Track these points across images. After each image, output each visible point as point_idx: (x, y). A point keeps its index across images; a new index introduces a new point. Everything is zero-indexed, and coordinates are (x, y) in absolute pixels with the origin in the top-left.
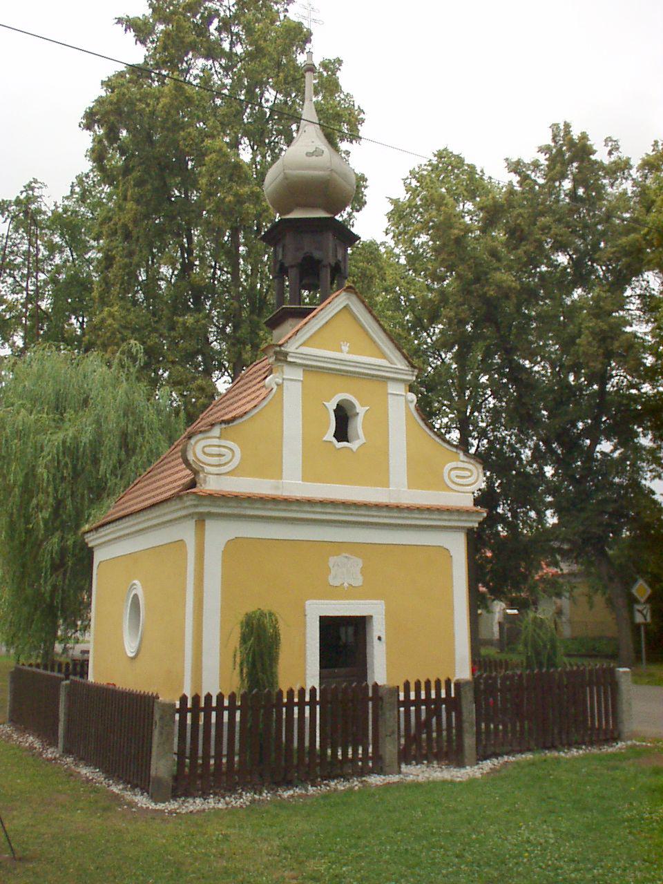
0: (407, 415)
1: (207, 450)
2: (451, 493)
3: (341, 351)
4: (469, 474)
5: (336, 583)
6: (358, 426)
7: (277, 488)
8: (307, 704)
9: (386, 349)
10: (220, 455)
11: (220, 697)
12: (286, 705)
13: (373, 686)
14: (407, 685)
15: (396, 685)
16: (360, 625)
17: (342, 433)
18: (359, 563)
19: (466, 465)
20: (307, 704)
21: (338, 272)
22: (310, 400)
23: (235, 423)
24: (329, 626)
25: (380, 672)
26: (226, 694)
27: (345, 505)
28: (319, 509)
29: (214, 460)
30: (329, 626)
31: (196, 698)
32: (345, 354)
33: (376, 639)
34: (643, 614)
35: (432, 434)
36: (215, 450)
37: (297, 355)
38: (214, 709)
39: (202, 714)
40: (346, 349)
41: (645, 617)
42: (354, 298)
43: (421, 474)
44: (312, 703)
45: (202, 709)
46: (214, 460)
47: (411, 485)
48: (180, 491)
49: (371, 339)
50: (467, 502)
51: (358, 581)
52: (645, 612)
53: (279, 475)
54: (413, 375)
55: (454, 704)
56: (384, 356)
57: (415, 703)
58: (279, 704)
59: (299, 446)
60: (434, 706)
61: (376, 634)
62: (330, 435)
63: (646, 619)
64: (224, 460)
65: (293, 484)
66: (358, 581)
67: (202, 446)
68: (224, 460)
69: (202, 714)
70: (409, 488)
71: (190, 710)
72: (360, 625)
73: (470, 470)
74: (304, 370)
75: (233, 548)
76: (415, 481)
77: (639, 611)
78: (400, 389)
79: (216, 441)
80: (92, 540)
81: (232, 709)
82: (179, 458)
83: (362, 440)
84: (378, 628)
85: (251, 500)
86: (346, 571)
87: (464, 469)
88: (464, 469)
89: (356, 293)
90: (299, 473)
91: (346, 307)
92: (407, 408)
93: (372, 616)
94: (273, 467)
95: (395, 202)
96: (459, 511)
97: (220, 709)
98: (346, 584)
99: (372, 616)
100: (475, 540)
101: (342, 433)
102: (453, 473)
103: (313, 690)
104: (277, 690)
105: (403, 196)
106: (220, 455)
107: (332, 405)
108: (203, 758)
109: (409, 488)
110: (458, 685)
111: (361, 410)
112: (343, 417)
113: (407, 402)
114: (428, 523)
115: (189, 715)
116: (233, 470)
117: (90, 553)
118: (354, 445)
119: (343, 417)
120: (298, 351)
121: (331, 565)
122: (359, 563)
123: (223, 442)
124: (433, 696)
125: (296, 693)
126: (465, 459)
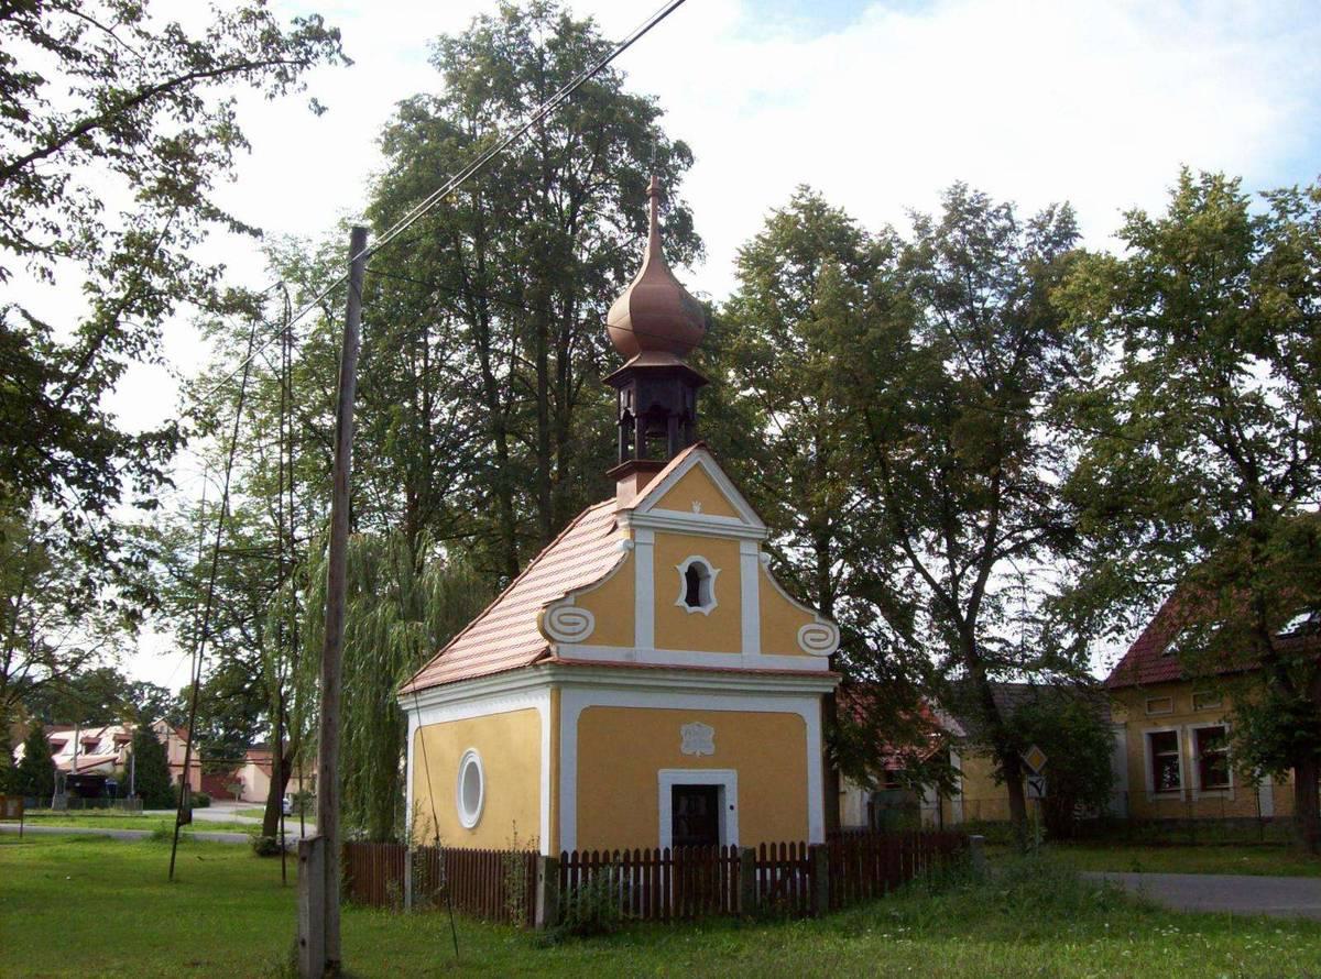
0: (760, 579)
1: (563, 618)
2: (804, 658)
6: (710, 588)
7: (629, 655)
9: (738, 508)
10: (575, 624)
11: (575, 854)
12: (653, 864)
15: (750, 847)
17: (694, 598)
19: (822, 628)
21: (688, 419)
22: (732, 615)
25: (732, 833)
28: (671, 676)
33: (728, 807)
36: (571, 619)
38: (570, 866)
40: (697, 508)
41: (1039, 791)
42: (706, 455)
43: (775, 637)
48: (536, 660)
49: (722, 495)
52: (1039, 784)
55: (807, 867)
56: (736, 514)
60: (788, 867)
62: (681, 601)
64: (578, 628)
65: (646, 650)
68: (578, 628)
69: (569, 870)
72: (712, 793)
73: (824, 632)
76: (767, 647)
77: (1031, 783)
79: (571, 610)
80: (406, 704)
82: (531, 621)
83: (714, 604)
84: (731, 797)
87: (819, 631)
88: (819, 631)
89: (708, 450)
93: (723, 786)
99: (723, 786)
100: (828, 702)
101: (694, 598)
102: (809, 636)
103: (667, 850)
105: (657, 121)
106: (575, 624)
107: (683, 568)
110: (813, 849)
111: (713, 572)
113: (760, 562)
114: (777, 689)
117: (404, 716)
118: (706, 610)
119: (695, 577)
120: (651, 513)
121: (683, 733)
124: (768, 871)
125: (652, 853)
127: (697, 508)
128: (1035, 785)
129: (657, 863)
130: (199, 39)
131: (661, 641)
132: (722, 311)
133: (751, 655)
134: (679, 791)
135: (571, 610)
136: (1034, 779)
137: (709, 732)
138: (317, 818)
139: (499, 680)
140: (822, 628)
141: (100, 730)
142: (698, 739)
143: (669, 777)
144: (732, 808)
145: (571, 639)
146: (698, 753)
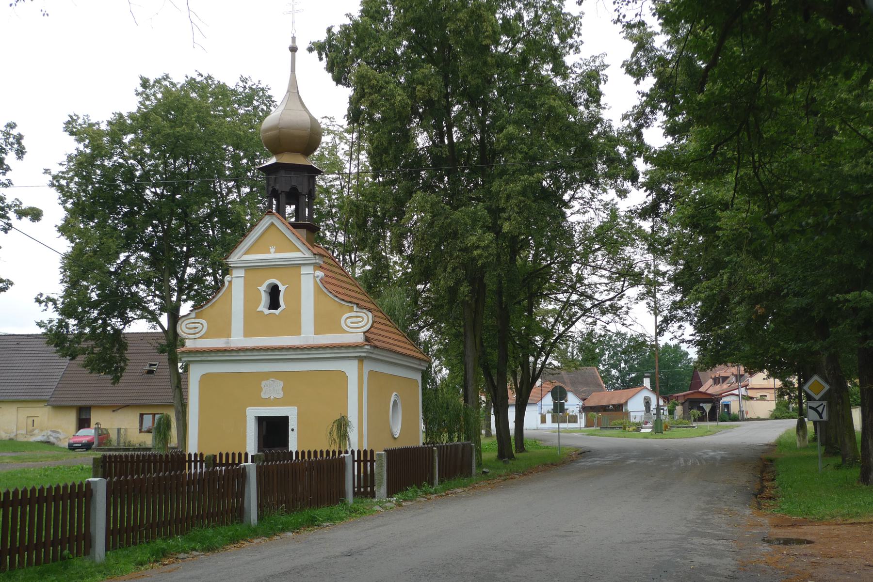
1: (188, 326)
5: (263, 396)
6: (265, 299)
8: (362, 461)
12: (204, 461)
14: (221, 455)
16: (283, 421)
17: (274, 304)
18: (282, 383)
19: (359, 314)
20: (369, 461)
24: (262, 421)
27: (281, 349)
29: (192, 331)
30: (262, 421)
32: (273, 255)
34: (817, 412)
35: (215, 300)
37: (236, 263)
38: (362, 461)
41: (820, 415)
45: (356, 461)
46: (192, 331)
47: (317, 332)
50: (359, 338)
51: (280, 395)
52: (820, 409)
53: (229, 336)
56: (299, 250)
58: (190, 461)
59: (242, 316)
61: (290, 428)
63: (821, 417)
64: (197, 330)
65: (238, 339)
66: (280, 395)
68: (197, 330)
70: (245, 336)
72: (283, 421)
74: (245, 270)
75: (205, 379)
76: (319, 330)
78: (309, 270)
79: (193, 320)
81: (196, 461)
84: (293, 424)
85: (217, 351)
86: (273, 389)
90: (312, 329)
91: (272, 224)
92: (315, 282)
94: (225, 331)
96: (356, 346)
98: (272, 397)
101: (274, 304)
106: (351, 323)
108: (358, 487)
109: (245, 336)
111: (282, 288)
112: (274, 292)
115: (198, 463)
119: (274, 292)
122: (282, 383)
123: (197, 320)
126: (358, 310)
127: (272, 250)
128: (815, 409)
129: (196, 461)
130: (259, 77)
131: (247, 333)
132: (656, 80)
133: (308, 335)
134: (261, 420)
135: (193, 320)
136: (814, 405)
137: (280, 384)
138: (808, 433)
139: (399, 357)
140: (359, 314)
141: (649, 388)
142: (273, 389)
143: (253, 413)
144: (293, 430)
145: (191, 336)
146: (272, 397)
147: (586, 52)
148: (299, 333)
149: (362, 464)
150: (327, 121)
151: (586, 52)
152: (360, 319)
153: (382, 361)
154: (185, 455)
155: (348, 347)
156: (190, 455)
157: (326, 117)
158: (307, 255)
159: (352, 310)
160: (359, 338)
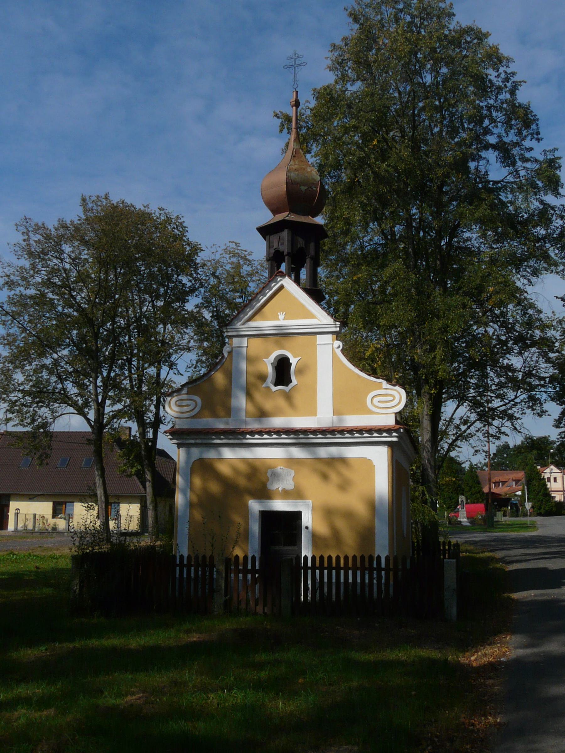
3: (279, 320)
4: (391, 398)
13: (304, 557)
20: (309, 568)
23: (198, 383)
26: (250, 556)
31: (197, 557)
39: (178, 568)
40: (281, 317)
44: (387, 569)
50: (390, 421)
54: (336, 327)
57: (248, 571)
67: (174, 402)
71: (342, 569)
78: (329, 338)
81: (346, 569)
95: (486, 35)
97: (189, 566)
102: (376, 400)
103: (254, 558)
104: (376, 555)
111: (293, 361)
116: (197, 413)
126: (389, 386)
127: (281, 317)
147: (546, 145)
148: (313, 413)
149: (334, 572)
150: (234, 245)
151: (546, 145)
152: (390, 398)
153: (126, 496)
154: (175, 557)
155: (380, 430)
156: (182, 557)
157: (233, 242)
158: (325, 322)
159: (380, 387)
160: (390, 421)
